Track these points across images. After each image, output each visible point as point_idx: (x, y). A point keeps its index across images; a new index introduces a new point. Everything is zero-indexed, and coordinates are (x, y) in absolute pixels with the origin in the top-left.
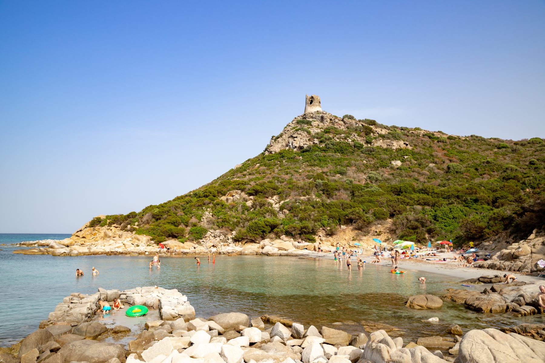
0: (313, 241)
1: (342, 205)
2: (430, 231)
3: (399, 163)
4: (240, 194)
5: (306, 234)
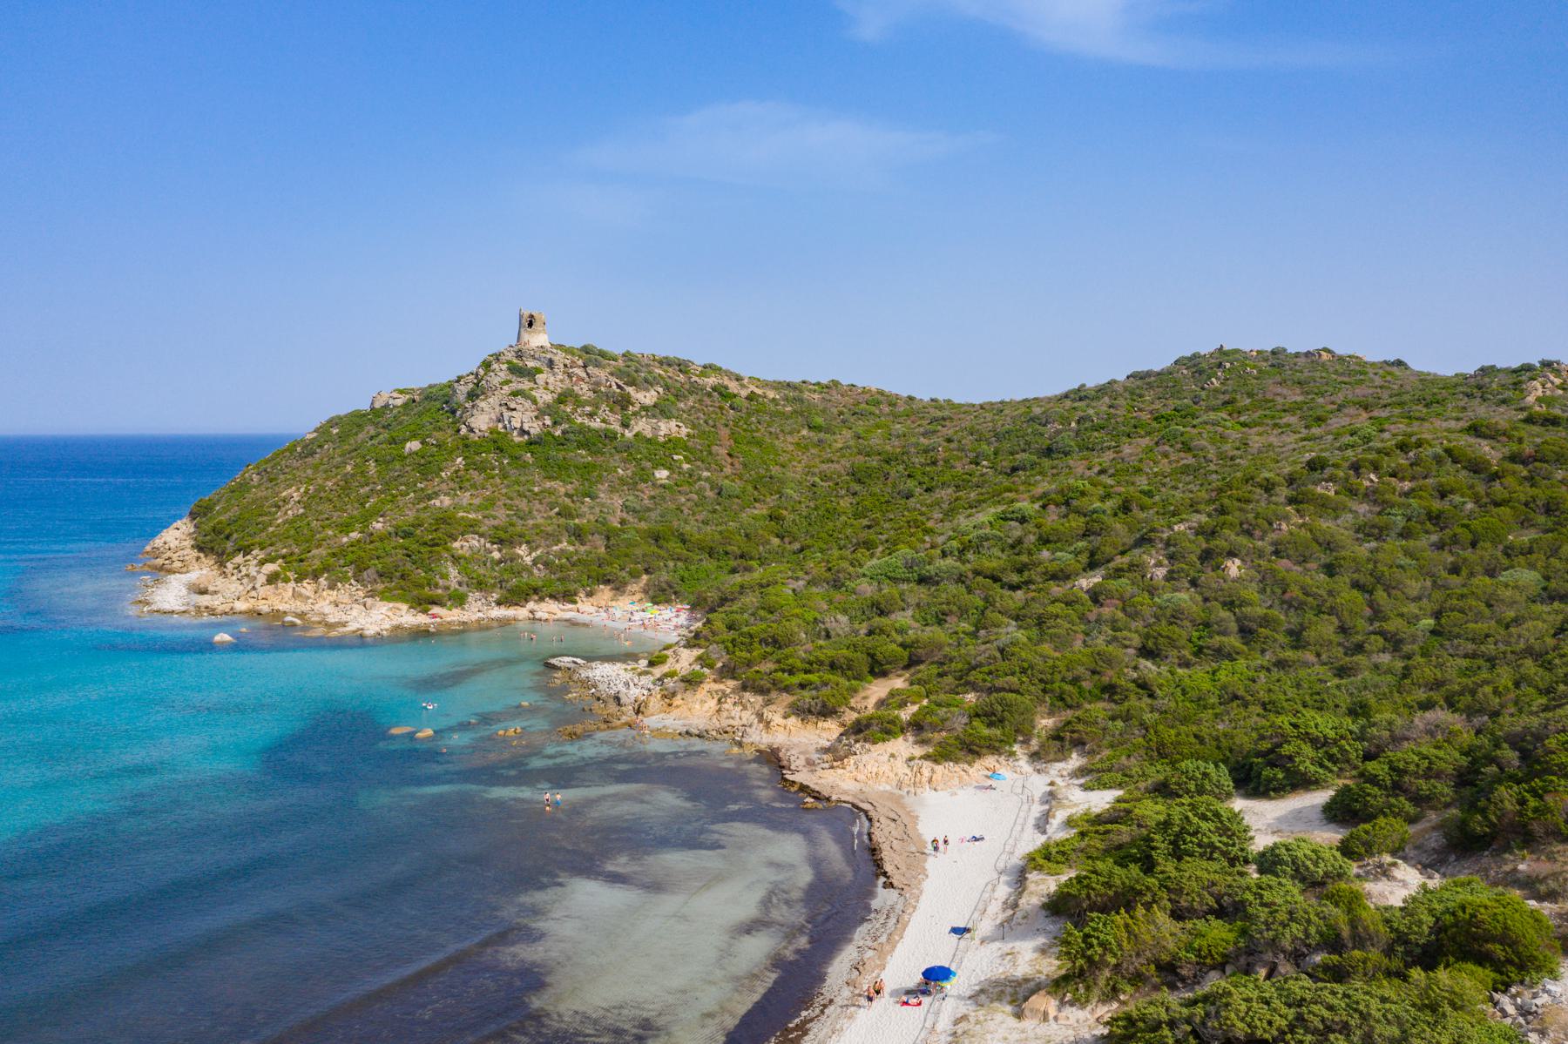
0: (575, 602)
3: (414, 445)
5: (568, 597)
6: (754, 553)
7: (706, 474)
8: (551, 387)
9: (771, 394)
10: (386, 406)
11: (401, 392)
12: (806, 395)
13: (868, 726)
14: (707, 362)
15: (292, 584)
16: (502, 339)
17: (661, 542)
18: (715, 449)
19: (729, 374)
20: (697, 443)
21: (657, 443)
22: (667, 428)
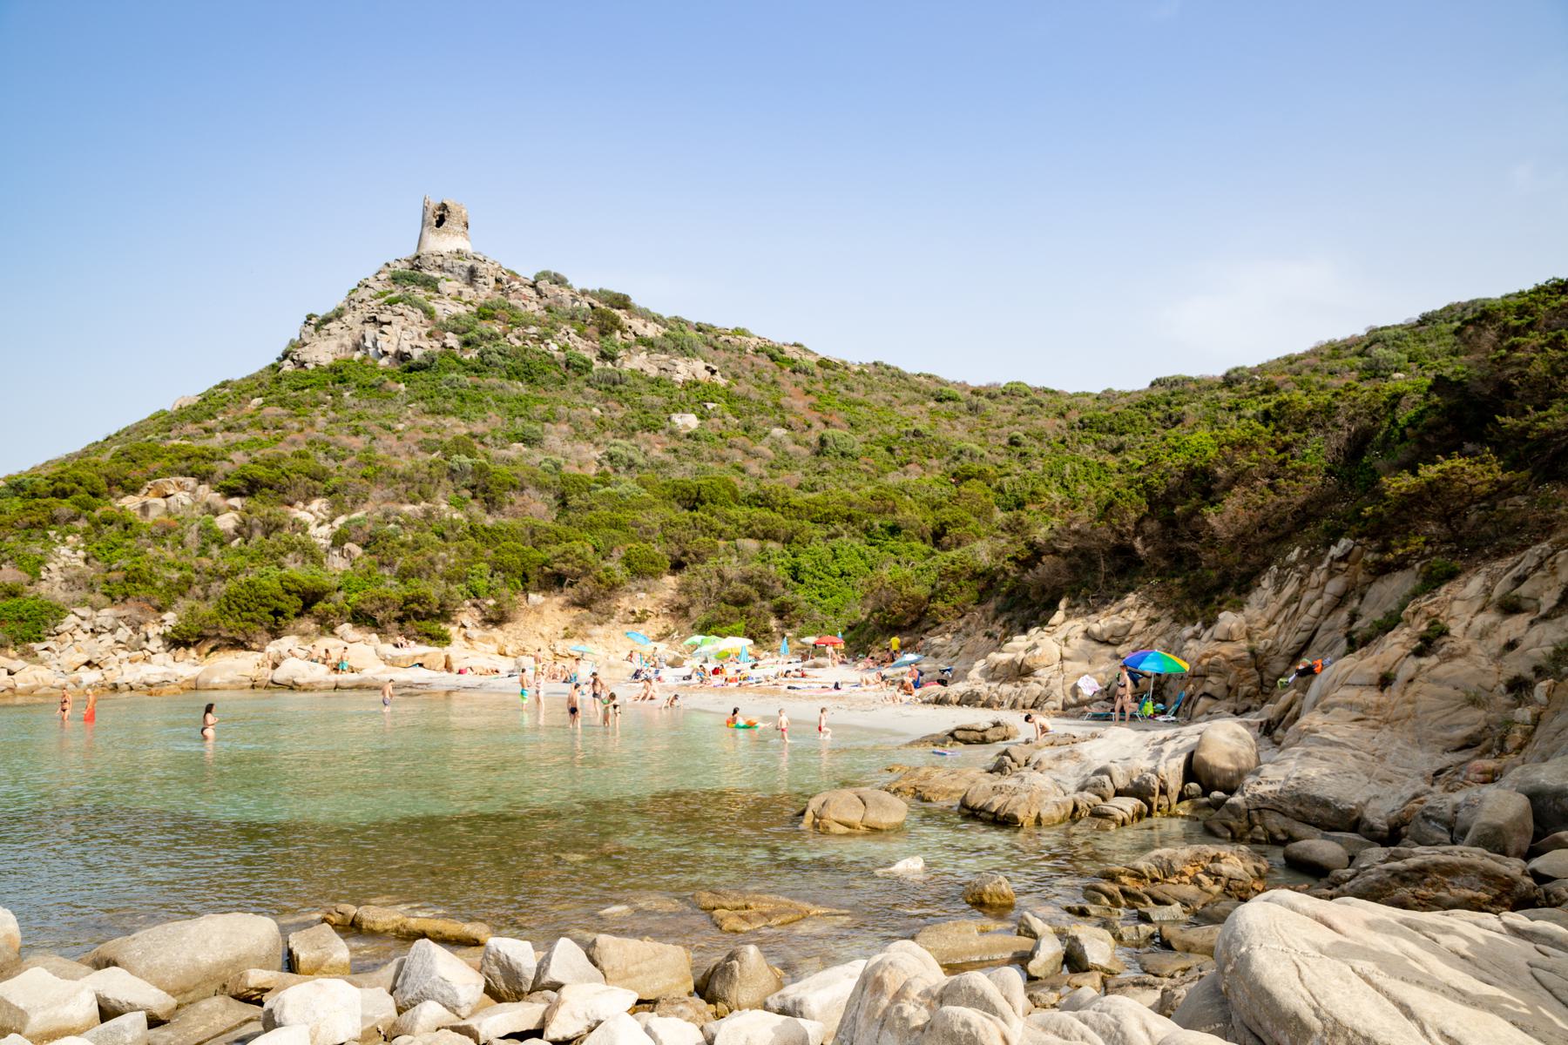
0: (442, 639)
1: (532, 534)
2: (781, 611)
5: (420, 618)
13: (1238, 381)
16: (399, 243)
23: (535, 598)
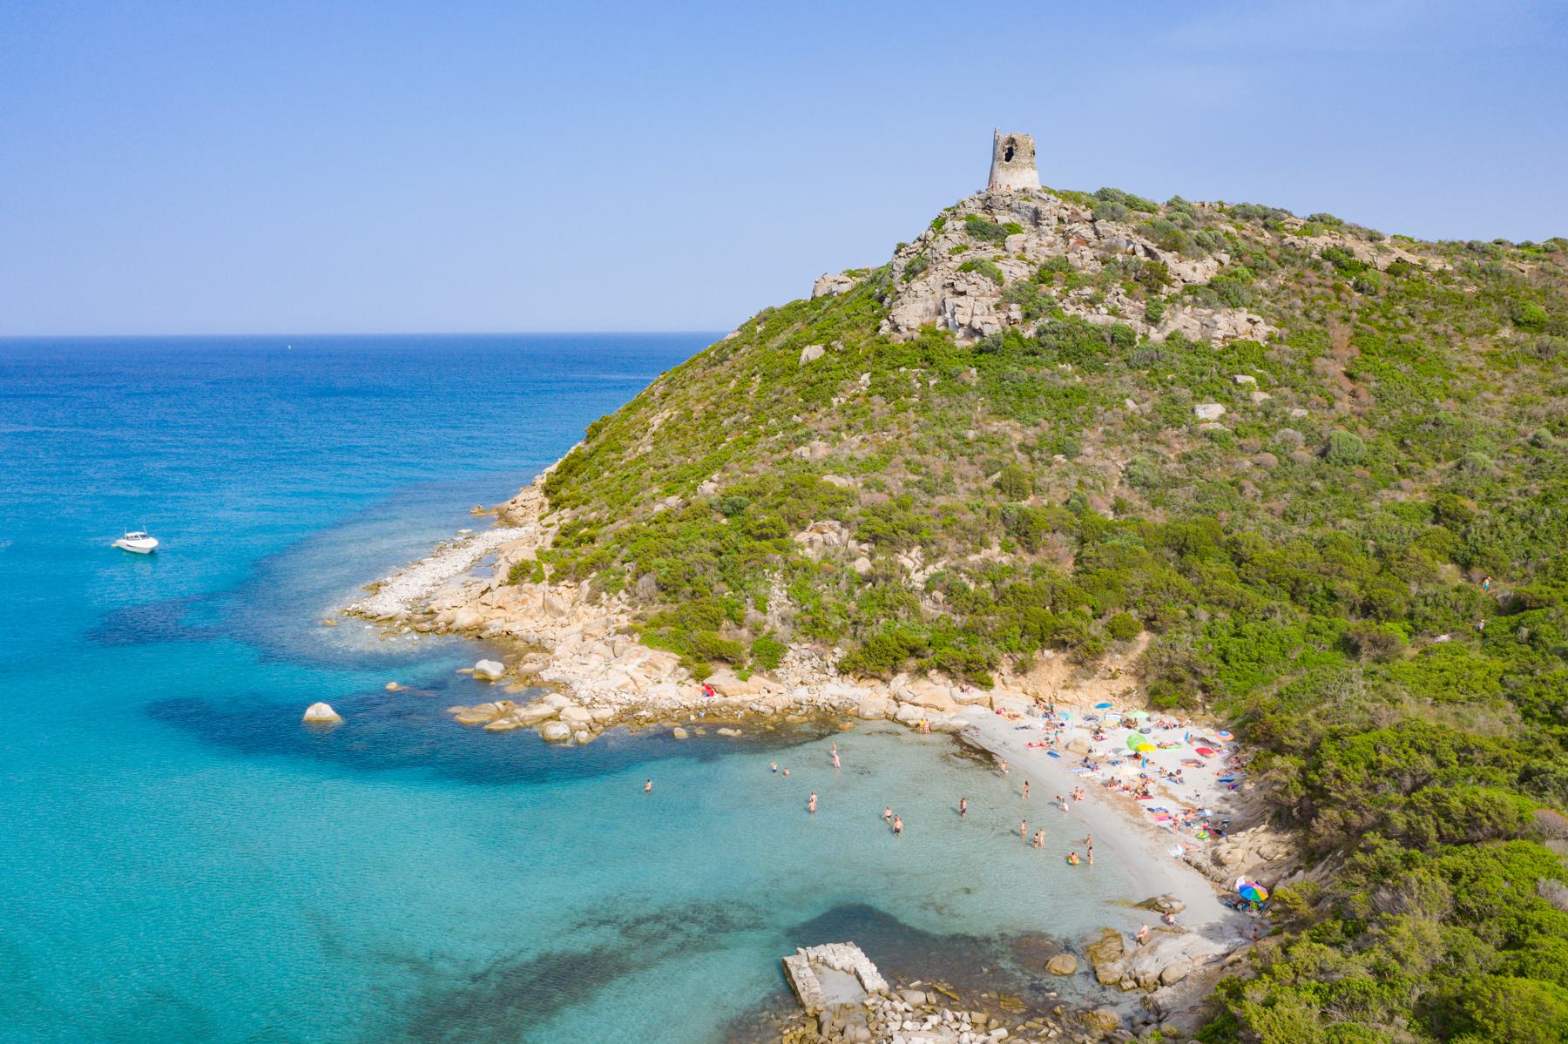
0: (987, 684)
1: (1053, 592)
2: (1204, 688)
4: (839, 533)
5: (974, 672)
6: (1398, 603)
7: (1298, 412)
8: (1029, 256)
9: (1436, 264)
10: (829, 295)
11: (851, 274)
12: (1505, 264)
14: (1316, 212)
15: (544, 586)
17: (1190, 557)
18: (1319, 363)
19: (1355, 231)
20: (1286, 352)
21: (1208, 352)
22: (1230, 324)
23: (1049, 653)
